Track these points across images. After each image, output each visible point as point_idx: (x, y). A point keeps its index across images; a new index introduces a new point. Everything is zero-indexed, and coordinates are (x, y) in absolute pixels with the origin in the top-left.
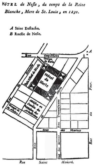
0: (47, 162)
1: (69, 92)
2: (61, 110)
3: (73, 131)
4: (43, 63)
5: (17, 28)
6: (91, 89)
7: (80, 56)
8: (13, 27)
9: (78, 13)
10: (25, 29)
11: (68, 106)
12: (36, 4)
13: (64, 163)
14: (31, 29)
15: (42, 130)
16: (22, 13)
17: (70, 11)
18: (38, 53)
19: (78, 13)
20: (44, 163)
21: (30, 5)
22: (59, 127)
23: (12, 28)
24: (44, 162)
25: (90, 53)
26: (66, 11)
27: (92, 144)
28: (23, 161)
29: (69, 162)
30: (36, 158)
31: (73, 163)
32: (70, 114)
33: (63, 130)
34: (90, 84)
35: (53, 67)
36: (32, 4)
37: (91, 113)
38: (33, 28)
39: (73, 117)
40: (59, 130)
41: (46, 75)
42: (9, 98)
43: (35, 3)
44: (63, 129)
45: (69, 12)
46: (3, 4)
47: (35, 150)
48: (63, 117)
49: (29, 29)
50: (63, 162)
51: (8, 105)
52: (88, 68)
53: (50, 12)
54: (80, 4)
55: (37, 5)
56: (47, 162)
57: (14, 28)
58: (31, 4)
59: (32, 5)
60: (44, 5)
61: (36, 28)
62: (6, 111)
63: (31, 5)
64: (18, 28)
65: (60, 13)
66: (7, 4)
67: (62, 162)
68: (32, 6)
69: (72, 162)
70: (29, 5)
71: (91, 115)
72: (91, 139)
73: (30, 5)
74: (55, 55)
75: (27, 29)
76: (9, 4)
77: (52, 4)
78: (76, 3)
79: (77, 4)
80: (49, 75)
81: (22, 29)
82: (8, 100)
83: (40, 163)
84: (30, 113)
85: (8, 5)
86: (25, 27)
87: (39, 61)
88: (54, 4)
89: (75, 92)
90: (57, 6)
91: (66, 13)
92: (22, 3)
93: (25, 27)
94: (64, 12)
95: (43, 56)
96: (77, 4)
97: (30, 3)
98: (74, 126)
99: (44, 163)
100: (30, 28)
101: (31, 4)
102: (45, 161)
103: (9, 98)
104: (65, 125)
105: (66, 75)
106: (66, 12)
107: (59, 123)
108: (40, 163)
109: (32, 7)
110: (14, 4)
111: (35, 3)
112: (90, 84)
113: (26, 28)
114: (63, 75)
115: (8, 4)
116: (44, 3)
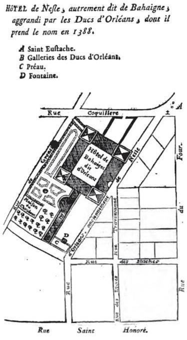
0: (93, 330)
3: (141, 261)
4: (82, 128)
7: (162, 111)
8: (23, 46)
10: (47, 51)
11: (135, 214)
13: (127, 332)
14: (59, 49)
15: (84, 262)
18: (74, 107)
21: (46, 10)
24: (88, 330)
26: (56, 31)
28: (45, 326)
29: (139, 330)
30: (72, 320)
31: (147, 332)
33: (124, 262)
35: (106, 136)
36: (51, 8)
38: (61, 48)
39: (146, 236)
40: (116, 261)
41: (90, 151)
47: (68, 280)
48: (125, 236)
50: (126, 331)
51: (15, 221)
52: (175, 135)
53: (78, 21)
54: (151, 6)
55: (61, 10)
56: (93, 330)
57: (26, 49)
58: (49, 7)
59: (52, 10)
62: (12, 226)
64: (34, 48)
67: (125, 330)
69: (145, 330)
70: (44, 10)
72: (182, 281)
73: (46, 10)
75: (50, 49)
77: (96, 8)
78: (133, 5)
79: (134, 5)
81: (42, 51)
84: (55, 192)
87: (76, 125)
88: (91, 8)
89: (149, 191)
95: (85, 113)
96: (135, 6)
97: (46, 7)
98: (147, 253)
101: (49, 7)
102: (90, 326)
104: (128, 252)
105: (130, 152)
107: (116, 246)
108: (79, 331)
114: (123, 151)
116: (110, 6)
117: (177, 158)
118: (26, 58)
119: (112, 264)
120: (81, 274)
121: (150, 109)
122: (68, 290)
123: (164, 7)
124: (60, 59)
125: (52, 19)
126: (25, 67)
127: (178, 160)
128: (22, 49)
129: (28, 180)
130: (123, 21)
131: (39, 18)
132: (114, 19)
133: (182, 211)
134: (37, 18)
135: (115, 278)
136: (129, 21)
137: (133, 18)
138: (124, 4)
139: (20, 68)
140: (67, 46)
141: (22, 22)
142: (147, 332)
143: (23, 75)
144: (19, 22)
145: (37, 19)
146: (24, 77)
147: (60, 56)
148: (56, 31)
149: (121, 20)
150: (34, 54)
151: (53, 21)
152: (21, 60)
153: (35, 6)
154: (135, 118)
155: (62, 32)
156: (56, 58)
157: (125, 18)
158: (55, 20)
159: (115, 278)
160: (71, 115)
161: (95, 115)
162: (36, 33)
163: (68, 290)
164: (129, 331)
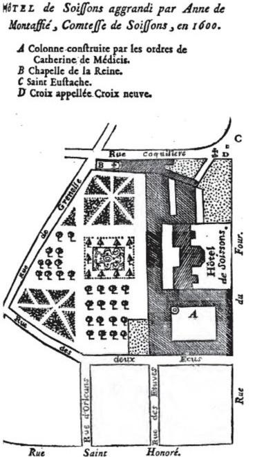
0: (105, 452)
6: (242, 253)
9: (242, 233)
10: (52, 85)
13: (152, 455)
14: (69, 83)
16: (173, 28)
17: (195, 24)
19: (217, 27)
20: (98, 454)
23: (21, 50)
27: (242, 403)
34: (239, 237)
37: (242, 296)
38: (72, 81)
42: (23, 267)
45: (193, 25)
46: (5, 8)
56: (105, 452)
64: (35, 80)
66: (13, 9)
69: (177, 452)
71: (241, 303)
75: (56, 83)
76: (17, 6)
82: (116, 152)
83: (87, 455)
85: (15, 11)
90: (161, 14)
92: (47, 5)
94: (180, 25)
99: (98, 454)
103: (23, 267)
106: (185, 27)
108: (86, 454)
110: (27, 8)
112: (239, 237)
113: (52, 82)
115: (15, 6)
117: (236, 252)
121: (53, 446)
123: (208, 8)
124: (72, 73)
125: (169, 8)
126: (25, 82)
127: (237, 254)
131: (150, 6)
133: (242, 301)
134: (147, 5)
136: (160, 28)
139: (20, 84)
141: (126, 11)
142: (179, 455)
143: (22, 91)
144: (120, 11)
145: (148, 7)
146: (23, 95)
147: (72, 70)
151: (171, 10)
152: (19, 73)
153: (219, 4)
156: (54, 94)
158: (175, 10)
164: (155, 453)
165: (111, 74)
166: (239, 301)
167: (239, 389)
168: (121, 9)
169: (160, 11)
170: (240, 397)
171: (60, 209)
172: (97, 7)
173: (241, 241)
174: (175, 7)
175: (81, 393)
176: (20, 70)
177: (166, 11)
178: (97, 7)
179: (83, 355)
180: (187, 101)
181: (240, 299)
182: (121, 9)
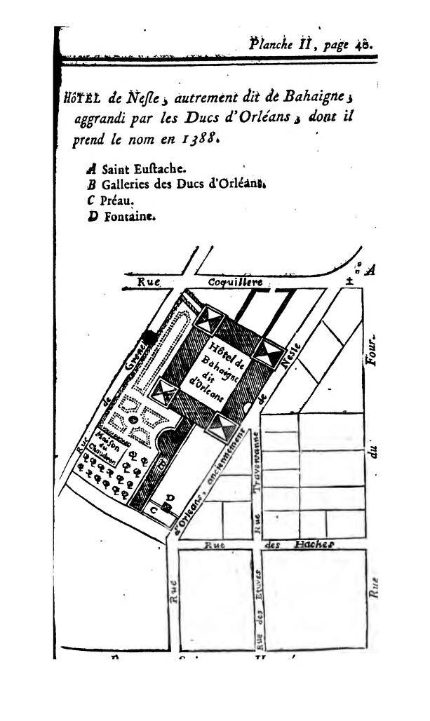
1: (297, 411)
2: (302, 537)
3: (304, 545)
5: (107, 168)
10: (136, 173)
12: (157, 97)
14: (157, 170)
17: (186, 137)
21: (135, 101)
22: (259, 532)
25: (370, 276)
26: (153, 138)
32: (300, 487)
33: (272, 546)
34: (371, 343)
40: (258, 545)
41: (213, 349)
43: (152, 93)
44: (272, 542)
48: (273, 499)
49: (147, 172)
52: (362, 321)
55: (161, 101)
57: (99, 169)
58: (140, 96)
60: (179, 102)
61: (173, 170)
63: (141, 99)
64: (114, 167)
65: (298, 121)
68: (144, 104)
70: (132, 100)
71: (374, 456)
73: (135, 101)
74: (248, 279)
75: (142, 170)
77: (223, 96)
80: (223, 348)
82: (80, 446)
86: (136, 166)
90: (76, 146)
91: (152, 143)
93: (136, 166)
95: (204, 281)
97: (135, 95)
98: (313, 529)
100: (151, 168)
101: (140, 96)
104: (275, 528)
106: (172, 139)
109: (143, 106)
111: (152, 93)
112: (371, 343)
113: (137, 169)
114: (270, 349)
117: (367, 362)
118: (98, 185)
119: (251, 550)
120: (197, 567)
122: (173, 594)
123: (342, 95)
124: (159, 187)
125: (145, 117)
126: (97, 200)
128: (92, 170)
129: (103, 399)
130: (270, 120)
131: (122, 115)
132: (254, 116)
133: (376, 454)
135: (256, 574)
136: (282, 120)
137: (288, 115)
138: (273, 90)
139: (89, 203)
140: (171, 164)
143: (94, 215)
147: (159, 183)
148: (153, 138)
149: (268, 118)
150: (113, 178)
152: (89, 189)
153: (115, 93)
154: (291, 292)
155: (163, 139)
157: (274, 115)
159: (256, 574)
160: (179, 285)
161: (220, 286)
162: (116, 141)
163: (173, 594)
165: (141, 219)
166: (372, 454)
167: (374, 579)
168: (88, 120)
169: (133, 122)
170: (375, 590)
171: (127, 369)
172: (282, 115)
173: (373, 348)
174: (152, 116)
175: (221, 453)
176: (91, 184)
177: (141, 122)
178: (282, 115)
179: (167, 537)
180: (310, 208)
181: (373, 452)
182: (88, 120)
